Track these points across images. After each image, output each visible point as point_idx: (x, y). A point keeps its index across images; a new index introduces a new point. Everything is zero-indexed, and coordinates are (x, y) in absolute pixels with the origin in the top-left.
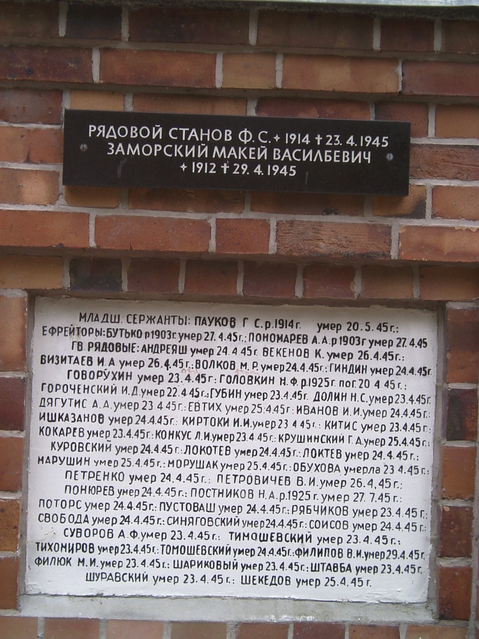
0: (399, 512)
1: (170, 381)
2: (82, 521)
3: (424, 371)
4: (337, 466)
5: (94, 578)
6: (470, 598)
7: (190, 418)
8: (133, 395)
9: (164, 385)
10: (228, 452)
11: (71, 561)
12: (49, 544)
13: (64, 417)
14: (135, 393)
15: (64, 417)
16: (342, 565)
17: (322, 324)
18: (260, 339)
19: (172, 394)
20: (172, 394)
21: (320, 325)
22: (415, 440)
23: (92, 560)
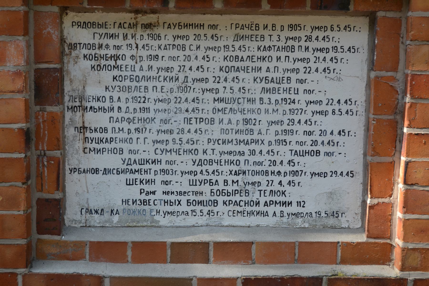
0: (282, 162)
1: (175, 103)
2: (132, 163)
3: (350, 174)
4: (267, 212)
5: (231, 102)
6: (49, 234)
7: (170, 77)
8: (126, 112)
9: (172, 105)
10: (257, 28)
11: (285, 193)
12: (178, 200)
13: (104, 140)
14: (127, 111)
15: (104, 140)
16: (211, 181)
17: (207, 47)
18: (91, 26)
19: (177, 102)
20: (177, 102)
21: (206, 47)
22: (349, 111)
23: (307, 47)
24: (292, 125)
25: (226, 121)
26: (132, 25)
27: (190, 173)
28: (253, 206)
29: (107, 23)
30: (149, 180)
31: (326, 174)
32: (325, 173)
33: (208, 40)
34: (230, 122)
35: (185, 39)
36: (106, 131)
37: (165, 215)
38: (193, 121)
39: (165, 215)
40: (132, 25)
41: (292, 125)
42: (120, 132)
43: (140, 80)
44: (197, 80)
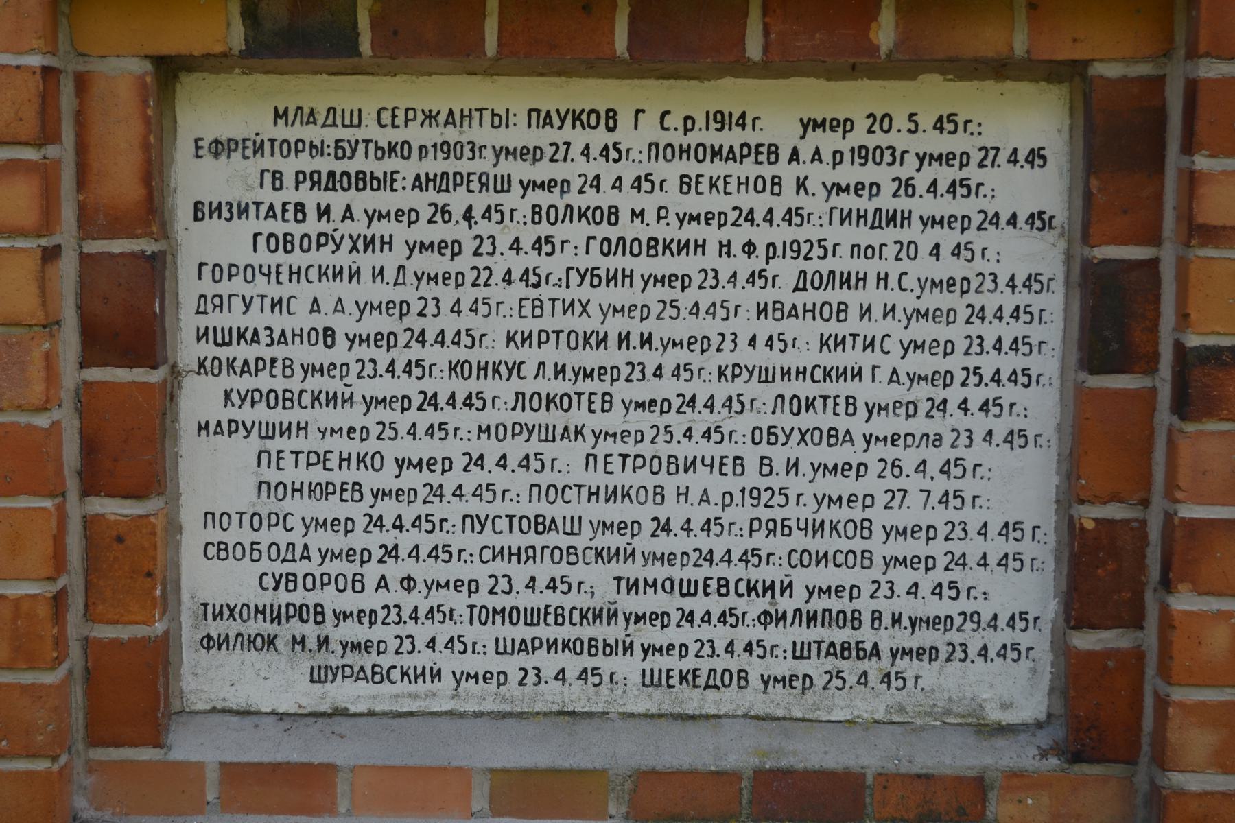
8: (396, 284)
24: (712, 287)
25: (337, 212)
26: (423, 179)
27: (388, 309)
28: (828, 320)
29: (395, 176)
30: (688, 241)
31: (686, 279)
32: (683, 276)
33: (675, 441)
34: (348, 214)
35: (557, 190)
36: (842, 316)
37: (909, 320)
38: (289, 459)
39: (909, 320)
40: (423, 179)
41: (712, 287)
42: (279, 121)
43: (561, 217)
44: (830, 499)
